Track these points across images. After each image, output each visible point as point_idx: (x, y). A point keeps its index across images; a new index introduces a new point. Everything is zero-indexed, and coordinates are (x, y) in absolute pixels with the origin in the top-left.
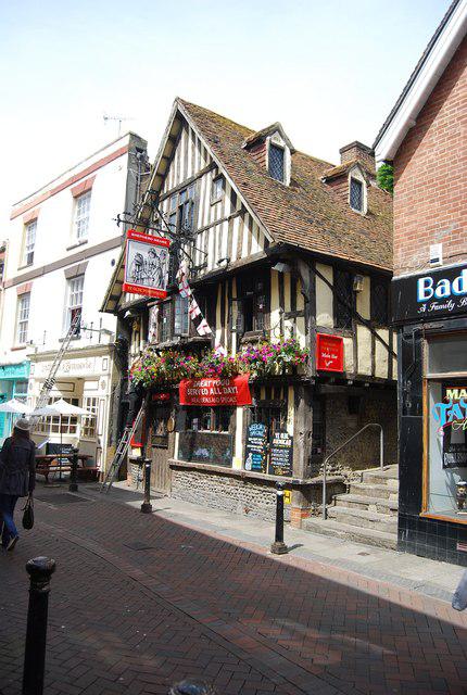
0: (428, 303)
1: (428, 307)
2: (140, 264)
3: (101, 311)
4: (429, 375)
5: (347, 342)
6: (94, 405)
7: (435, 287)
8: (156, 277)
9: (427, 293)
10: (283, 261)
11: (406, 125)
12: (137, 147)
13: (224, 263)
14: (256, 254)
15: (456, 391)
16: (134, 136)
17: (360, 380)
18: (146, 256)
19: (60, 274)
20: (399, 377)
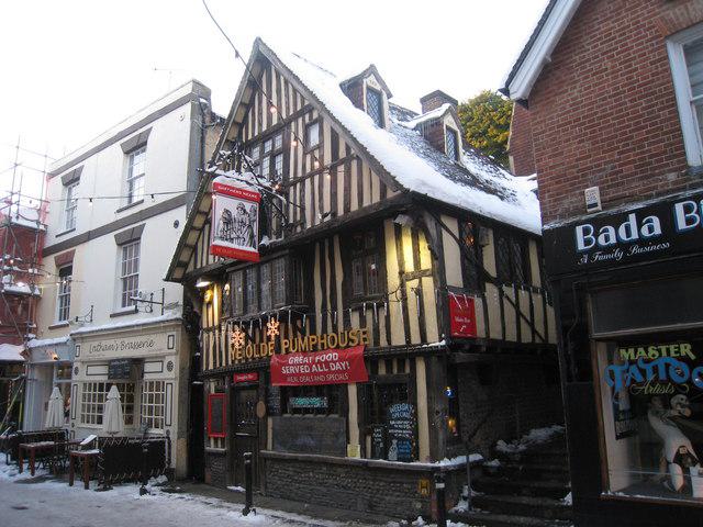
0: (590, 253)
1: (590, 258)
2: (228, 221)
3: (167, 279)
4: (596, 335)
5: (478, 302)
7: (596, 235)
9: (587, 242)
10: (404, 213)
12: (198, 99)
13: (328, 219)
14: (370, 207)
15: (631, 351)
16: (196, 83)
17: (493, 345)
18: (235, 213)
19: (110, 239)
20: (559, 338)
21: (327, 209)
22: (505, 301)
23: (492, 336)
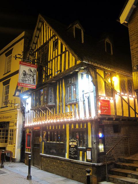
6: (13, 132)
8: (32, 80)
11: (132, 8)
13: (59, 72)
17: (118, 118)
18: (27, 72)
21: (59, 69)
22: (123, 101)
23: (118, 114)
